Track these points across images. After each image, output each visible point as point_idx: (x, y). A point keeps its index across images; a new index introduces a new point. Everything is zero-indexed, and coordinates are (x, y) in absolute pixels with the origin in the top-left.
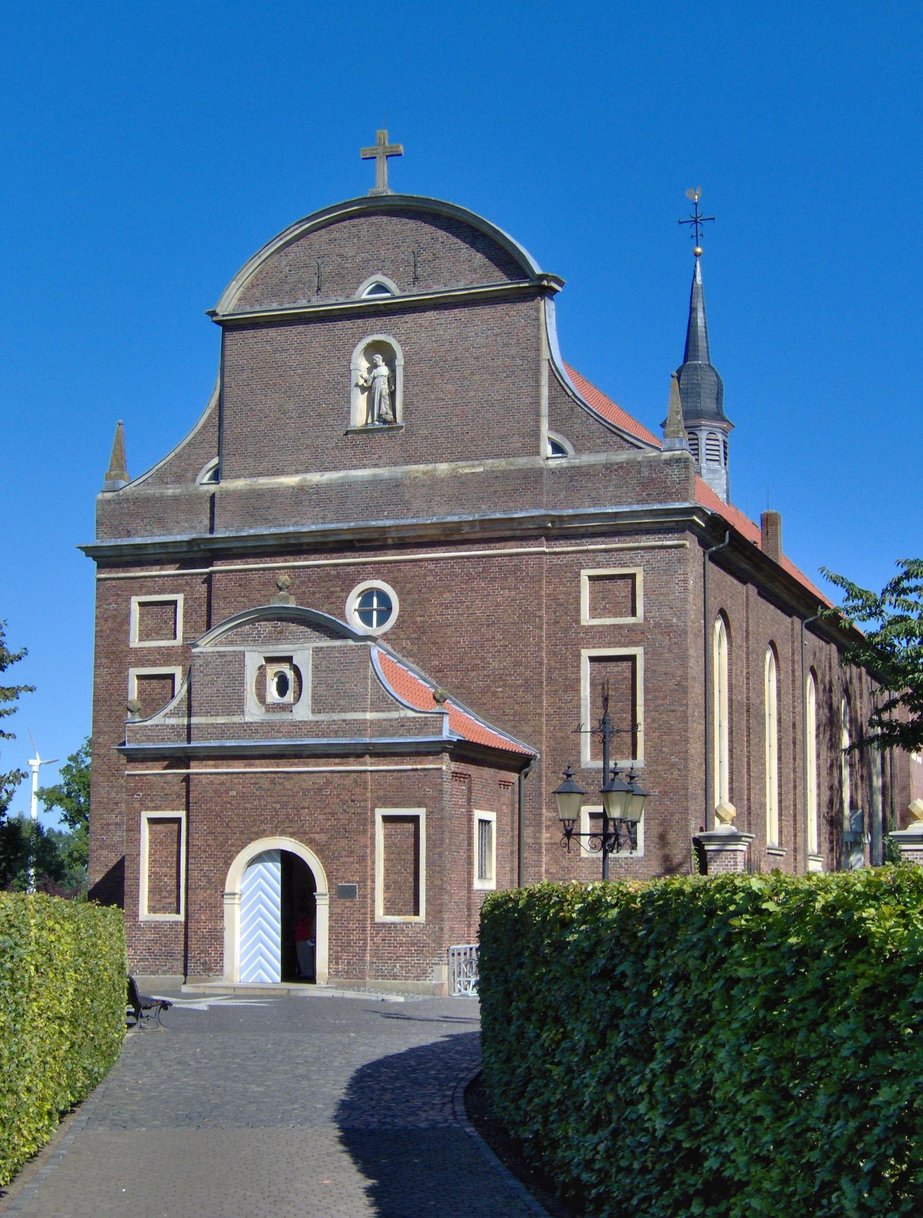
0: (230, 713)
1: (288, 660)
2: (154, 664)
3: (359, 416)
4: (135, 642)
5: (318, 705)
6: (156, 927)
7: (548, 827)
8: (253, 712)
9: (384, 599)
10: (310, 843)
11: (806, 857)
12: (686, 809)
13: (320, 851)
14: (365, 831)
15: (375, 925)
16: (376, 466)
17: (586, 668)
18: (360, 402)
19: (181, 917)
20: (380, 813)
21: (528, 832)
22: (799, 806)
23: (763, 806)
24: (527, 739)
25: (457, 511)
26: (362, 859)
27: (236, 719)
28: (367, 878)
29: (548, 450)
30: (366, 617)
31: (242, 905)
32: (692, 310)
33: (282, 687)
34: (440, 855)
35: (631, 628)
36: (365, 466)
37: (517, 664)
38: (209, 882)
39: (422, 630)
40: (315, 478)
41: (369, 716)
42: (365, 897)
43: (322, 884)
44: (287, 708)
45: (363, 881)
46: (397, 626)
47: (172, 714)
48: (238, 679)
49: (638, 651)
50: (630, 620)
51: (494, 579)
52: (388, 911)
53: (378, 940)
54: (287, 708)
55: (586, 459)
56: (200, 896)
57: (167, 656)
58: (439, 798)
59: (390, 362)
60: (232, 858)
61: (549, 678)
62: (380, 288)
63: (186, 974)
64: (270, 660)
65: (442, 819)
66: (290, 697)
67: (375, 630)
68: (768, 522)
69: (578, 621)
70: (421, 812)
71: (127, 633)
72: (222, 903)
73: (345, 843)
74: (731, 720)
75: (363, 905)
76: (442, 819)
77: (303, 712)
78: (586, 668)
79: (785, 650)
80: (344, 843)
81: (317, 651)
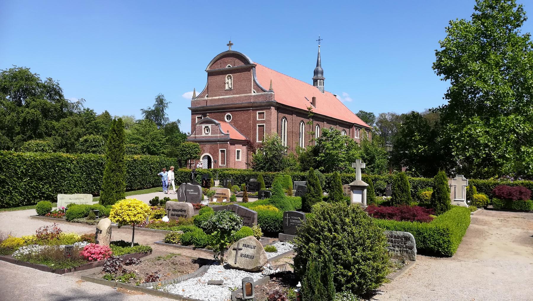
3: (227, 88)
8: (204, 135)
25: (33, 142)
28: (218, 159)
29: (253, 92)
43: (212, 160)
49: (264, 124)
55: (258, 94)
57: (263, 122)
59: (231, 78)
64: (206, 127)
67: (229, 121)
73: (215, 154)
77: (210, 135)
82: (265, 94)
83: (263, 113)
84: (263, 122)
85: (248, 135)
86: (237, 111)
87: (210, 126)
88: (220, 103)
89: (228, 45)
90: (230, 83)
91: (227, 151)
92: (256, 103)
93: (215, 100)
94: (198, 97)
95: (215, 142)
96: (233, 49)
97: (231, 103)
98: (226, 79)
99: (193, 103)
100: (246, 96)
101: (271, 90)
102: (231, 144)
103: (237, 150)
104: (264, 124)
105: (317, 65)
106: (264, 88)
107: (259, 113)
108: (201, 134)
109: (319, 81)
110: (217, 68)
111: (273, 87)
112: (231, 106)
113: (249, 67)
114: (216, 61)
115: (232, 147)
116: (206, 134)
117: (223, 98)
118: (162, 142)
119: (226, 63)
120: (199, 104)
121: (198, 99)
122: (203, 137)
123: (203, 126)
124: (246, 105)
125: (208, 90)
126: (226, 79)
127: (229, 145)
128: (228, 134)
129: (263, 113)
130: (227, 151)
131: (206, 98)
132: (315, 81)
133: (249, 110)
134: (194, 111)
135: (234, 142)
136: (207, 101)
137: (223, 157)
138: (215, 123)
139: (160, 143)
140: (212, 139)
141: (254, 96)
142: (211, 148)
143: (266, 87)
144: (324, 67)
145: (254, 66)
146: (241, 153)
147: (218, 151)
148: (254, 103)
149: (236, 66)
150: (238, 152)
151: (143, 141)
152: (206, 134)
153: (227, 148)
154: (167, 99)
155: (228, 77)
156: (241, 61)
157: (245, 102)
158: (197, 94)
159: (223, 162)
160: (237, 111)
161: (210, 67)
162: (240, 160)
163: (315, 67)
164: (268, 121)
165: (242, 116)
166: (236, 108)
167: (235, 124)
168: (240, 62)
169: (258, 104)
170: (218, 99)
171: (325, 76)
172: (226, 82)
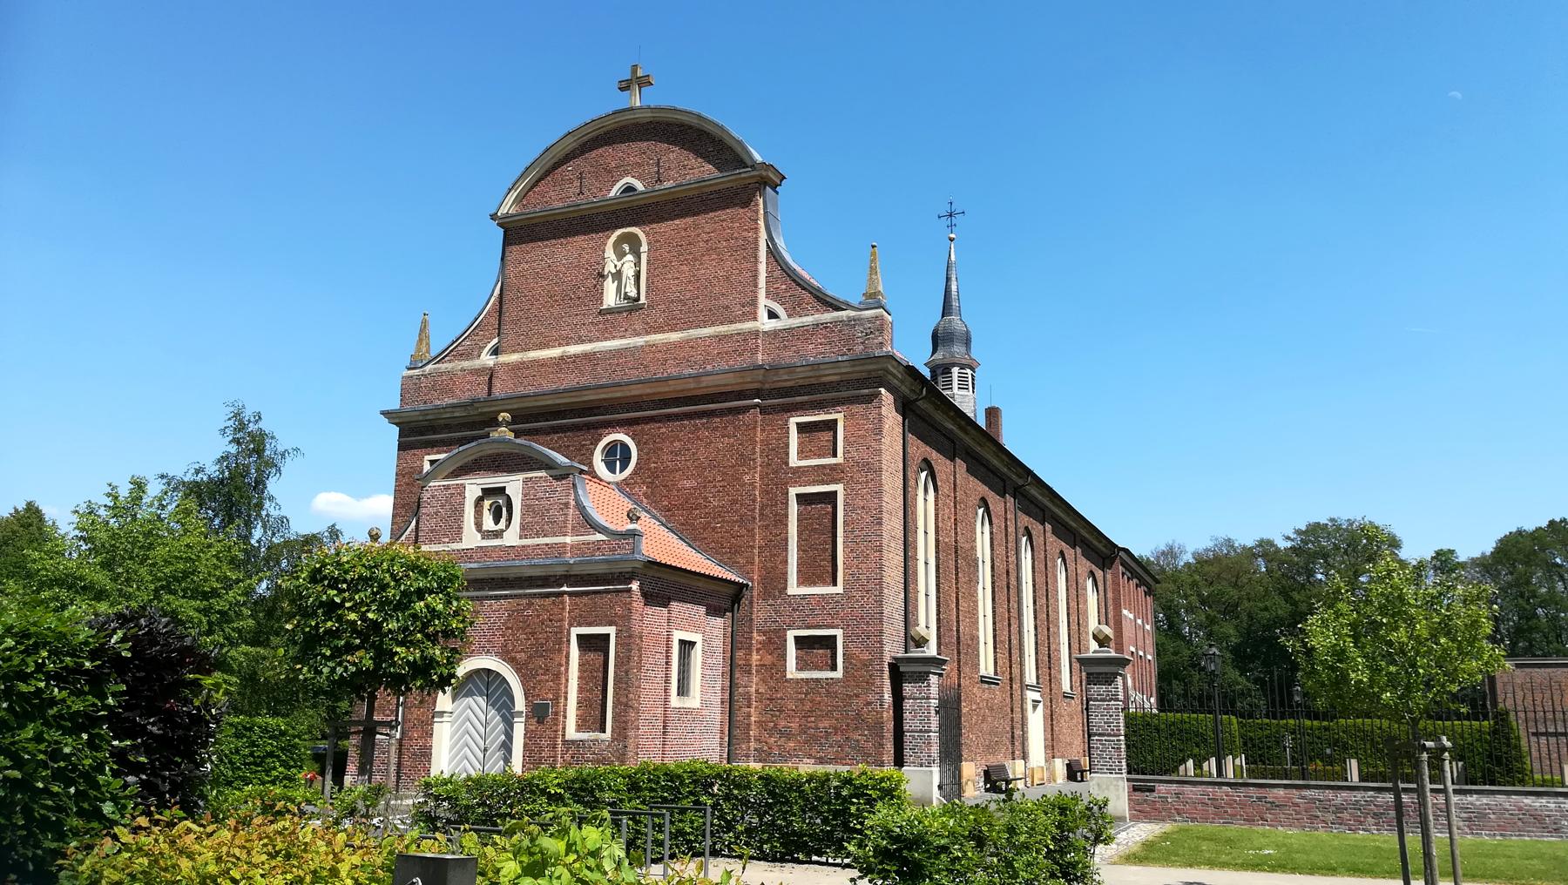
0: (453, 541)
3: (610, 298)
5: (525, 531)
7: (758, 650)
8: (471, 539)
9: (625, 447)
10: (511, 661)
11: (1024, 687)
12: (881, 632)
14: (560, 650)
15: (565, 742)
16: (623, 337)
21: (740, 654)
22: (1015, 642)
23: (975, 639)
24: (741, 570)
26: (557, 676)
27: (455, 546)
28: (559, 696)
29: (763, 314)
30: (611, 467)
31: (453, 723)
32: (948, 279)
34: (627, 672)
35: (833, 468)
36: (614, 338)
37: (734, 502)
39: (655, 475)
41: (568, 540)
42: (556, 714)
43: (520, 704)
44: (498, 534)
45: (556, 699)
46: (635, 473)
48: (458, 512)
49: (839, 488)
50: (832, 461)
52: (579, 729)
54: (498, 534)
55: (796, 322)
57: (831, 473)
58: (627, 617)
61: (761, 514)
64: (488, 492)
65: (630, 636)
68: (993, 413)
69: (787, 464)
70: (611, 631)
74: (937, 558)
75: (555, 722)
76: (630, 636)
77: (512, 538)
79: (1038, 540)
80: (541, 662)
81: (525, 481)
82: (835, 322)
83: (831, 426)
84: (831, 473)
85: (735, 550)
86: (669, 418)
87: (514, 485)
88: (570, 380)
89: (625, 86)
91: (626, 640)
92: (791, 368)
94: (440, 358)
95: (545, 581)
97: (634, 375)
98: (610, 253)
99: (409, 388)
100: (721, 338)
101: (873, 299)
102: (651, 598)
103: (678, 635)
104: (839, 488)
105: (947, 309)
106: (832, 291)
107: (802, 428)
108: (457, 534)
109: (955, 370)
110: (559, 198)
112: (636, 391)
113: (738, 182)
114: (551, 166)
115: (650, 619)
116: (487, 535)
117: (586, 356)
118: (219, 604)
119: (612, 175)
120: (447, 391)
121: (443, 366)
122: (467, 554)
123: (472, 487)
125: (501, 319)
126: (610, 253)
127: (638, 602)
128: (633, 534)
129: (831, 426)
130: (626, 640)
131: (487, 359)
133: (746, 409)
134: (416, 430)
135: (665, 585)
136: (491, 373)
137: (594, 680)
138: (549, 465)
139: (206, 611)
140: (522, 566)
141: (775, 334)
142: (517, 623)
144: (969, 317)
145: (767, 180)
146: (697, 655)
147: (561, 641)
148: (775, 369)
149: (667, 184)
150: (686, 646)
151: (100, 595)
152: (487, 535)
153: (623, 621)
154: (282, 432)
155: (617, 245)
156: (699, 154)
157: (720, 370)
158: (437, 345)
159: (593, 717)
160: (669, 418)
162: (694, 701)
163: (934, 318)
164: (865, 471)
165: (709, 443)
166: (666, 403)
167: (653, 488)
168: (693, 161)
169: (800, 377)
170: (554, 357)
171: (976, 352)
172: (610, 268)
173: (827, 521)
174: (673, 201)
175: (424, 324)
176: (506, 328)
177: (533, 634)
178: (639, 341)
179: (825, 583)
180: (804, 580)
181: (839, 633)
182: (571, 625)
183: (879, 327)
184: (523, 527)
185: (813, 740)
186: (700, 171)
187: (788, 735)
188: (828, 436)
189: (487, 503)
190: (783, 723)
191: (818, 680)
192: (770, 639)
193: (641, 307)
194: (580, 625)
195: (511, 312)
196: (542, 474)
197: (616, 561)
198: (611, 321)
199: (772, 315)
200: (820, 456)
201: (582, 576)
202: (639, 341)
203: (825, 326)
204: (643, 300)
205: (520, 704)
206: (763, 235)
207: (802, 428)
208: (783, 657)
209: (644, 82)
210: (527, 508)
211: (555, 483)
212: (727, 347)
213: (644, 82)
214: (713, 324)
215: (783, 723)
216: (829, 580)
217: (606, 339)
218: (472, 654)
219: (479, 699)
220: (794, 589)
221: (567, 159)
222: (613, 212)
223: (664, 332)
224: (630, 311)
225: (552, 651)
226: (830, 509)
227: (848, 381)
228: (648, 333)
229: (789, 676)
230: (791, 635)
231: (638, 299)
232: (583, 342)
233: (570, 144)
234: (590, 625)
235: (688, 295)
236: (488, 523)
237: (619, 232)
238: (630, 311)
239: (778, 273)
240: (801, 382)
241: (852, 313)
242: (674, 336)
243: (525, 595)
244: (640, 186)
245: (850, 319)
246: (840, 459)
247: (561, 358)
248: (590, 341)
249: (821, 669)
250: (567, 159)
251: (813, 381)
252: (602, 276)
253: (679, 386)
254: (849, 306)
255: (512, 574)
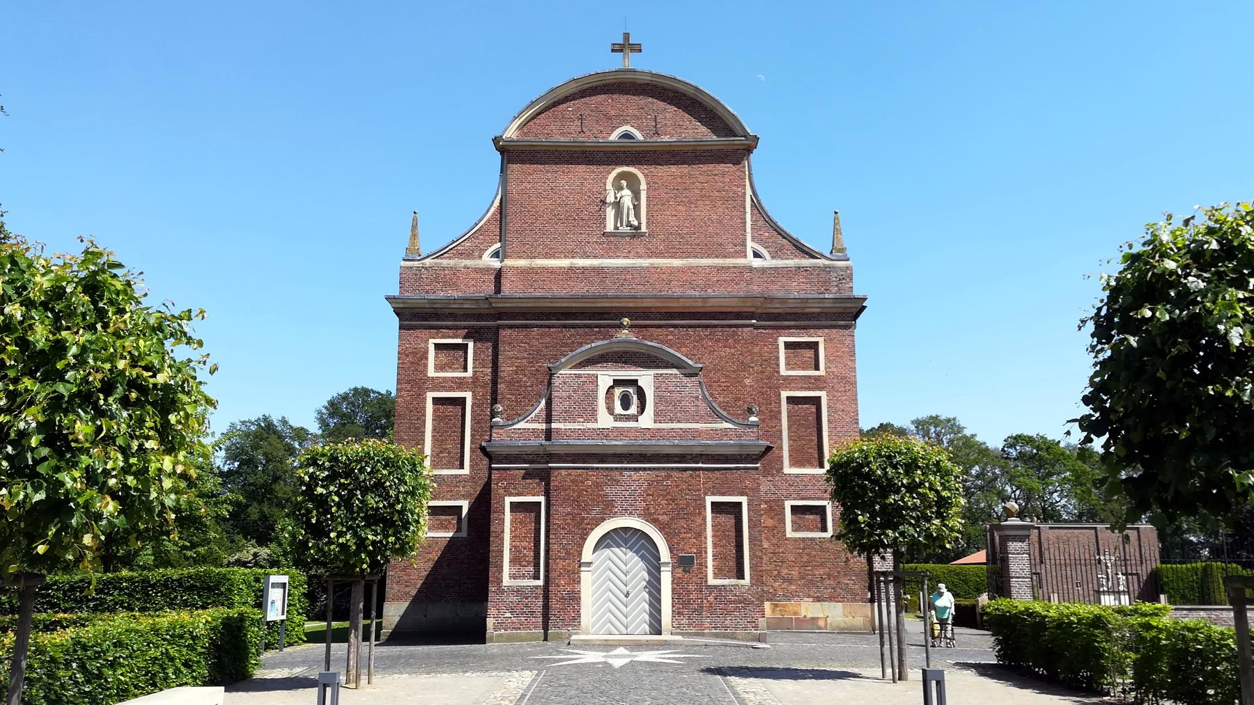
0: (587, 421)
1: (634, 383)
2: (451, 389)
4: (431, 373)
5: (658, 416)
6: (519, 591)
8: (605, 421)
10: (655, 522)
13: (662, 527)
14: (700, 514)
17: (784, 406)
18: (610, 213)
19: (541, 582)
20: (710, 499)
27: (591, 425)
28: (702, 551)
29: (750, 253)
33: (626, 403)
35: (817, 379)
36: (618, 257)
37: (738, 399)
38: (568, 553)
40: (581, 262)
43: (665, 555)
47: (533, 421)
49: (823, 394)
51: (718, 341)
53: (711, 598)
54: (635, 418)
56: (559, 565)
57: (817, 383)
60: (587, 534)
62: (627, 136)
63: (546, 627)
64: (618, 383)
66: (633, 410)
70: (744, 500)
71: (426, 366)
72: (579, 572)
77: (647, 420)
78: (784, 406)
80: (683, 523)
81: (656, 376)
82: (814, 268)
84: (817, 383)
87: (646, 378)
88: (580, 288)
90: (627, 201)
93: (552, 271)
96: (642, 64)
100: (720, 269)
101: (838, 250)
107: (788, 345)
108: (593, 416)
110: (561, 132)
111: (846, 241)
113: (729, 144)
120: (448, 284)
121: (445, 262)
122: (604, 433)
123: (605, 377)
124: (732, 305)
131: (488, 261)
132: (216, 369)
136: (499, 274)
138: (678, 365)
140: (664, 445)
143: (821, 244)
149: (666, 138)
152: (618, 418)
157: (722, 294)
161: (521, 127)
169: (790, 307)
170: (551, 267)
172: (610, 198)
173: (812, 418)
174: (669, 152)
175: (415, 220)
176: (511, 237)
177: (673, 500)
178: (645, 262)
179: (812, 466)
180: (795, 462)
181: (744, 500)
182: (706, 494)
183: (847, 275)
184: (656, 414)
185: (811, 584)
186: (697, 132)
187: (789, 581)
188: (809, 353)
189: (618, 392)
190: (785, 571)
191: (812, 539)
192: (771, 507)
193: (643, 235)
194: (713, 494)
195: (513, 224)
196: (675, 371)
197: (742, 446)
198: (612, 243)
199: (757, 255)
200: (803, 369)
201: (713, 456)
202: (645, 262)
203: (806, 269)
204: (644, 229)
205: (665, 555)
206: (749, 192)
207: (788, 345)
208: (783, 521)
209: (637, 48)
210: (659, 399)
211: (685, 380)
212: (724, 276)
213: (637, 48)
214: (709, 256)
215: (785, 571)
216: (816, 463)
217: (610, 257)
218: (615, 515)
219: (616, 550)
220: (788, 470)
221: (566, 99)
222: (613, 153)
223: (664, 257)
224: (633, 236)
225: (693, 514)
226: (813, 409)
227: (826, 314)
228: (650, 257)
229: (788, 535)
230: (788, 504)
231: (638, 228)
232: (588, 257)
233: (573, 88)
234: (723, 494)
235: (686, 230)
236: (618, 409)
237: (619, 170)
238: (633, 236)
239: (761, 223)
240: (789, 311)
241: (827, 262)
242: (677, 262)
243: (663, 469)
244: (639, 136)
245: (826, 267)
246: (822, 372)
247: (571, 268)
248: (595, 257)
249: (811, 530)
250: (566, 99)
251: (798, 311)
252: (604, 202)
253: (682, 303)
254: (811, 254)
255: (650, 451)
